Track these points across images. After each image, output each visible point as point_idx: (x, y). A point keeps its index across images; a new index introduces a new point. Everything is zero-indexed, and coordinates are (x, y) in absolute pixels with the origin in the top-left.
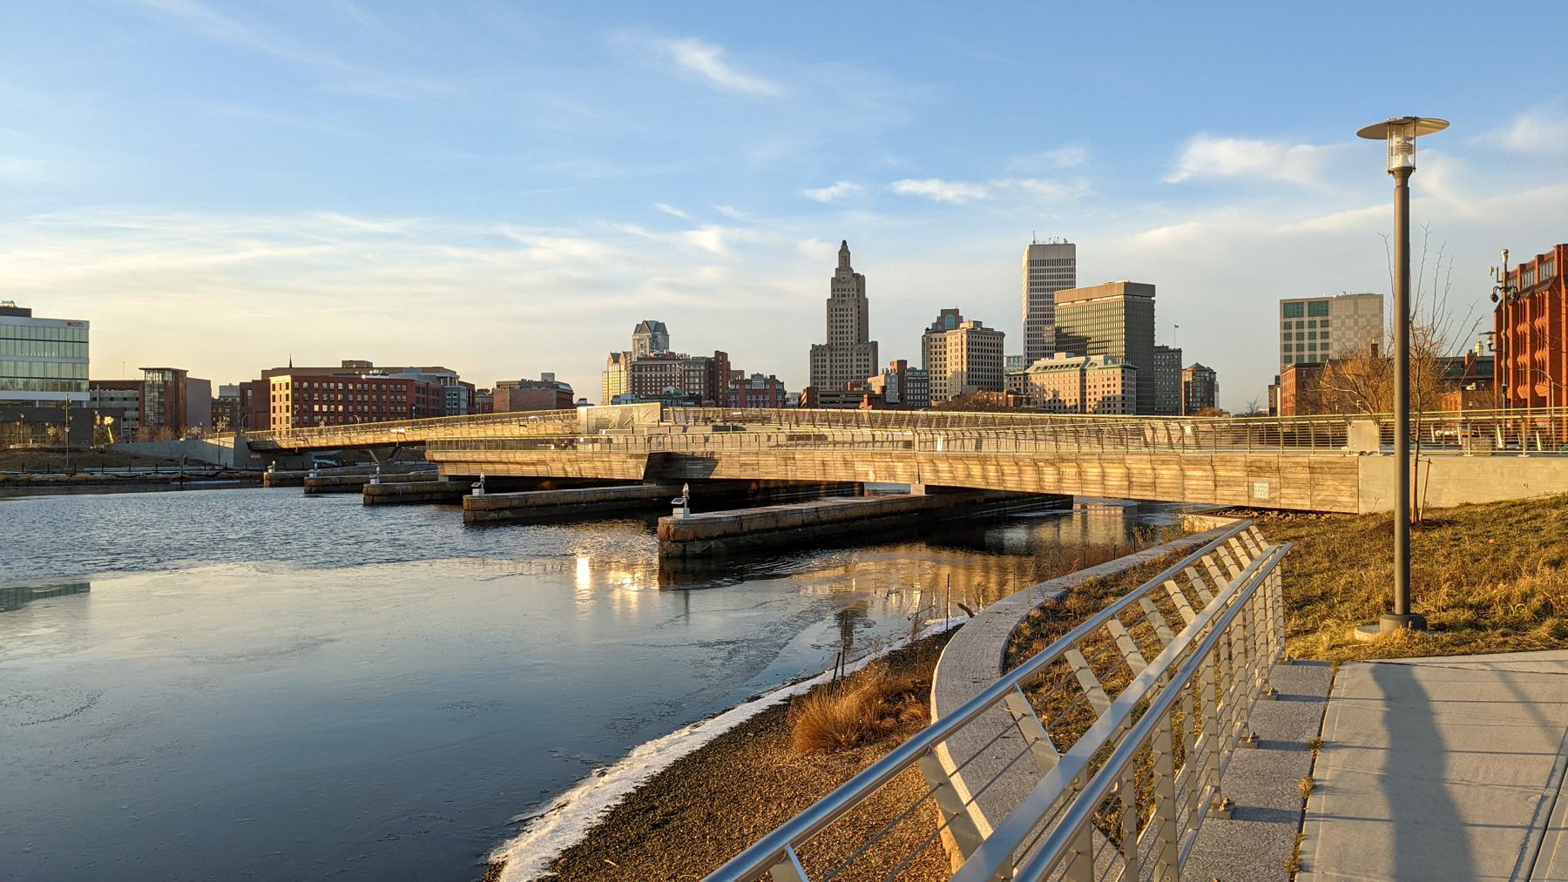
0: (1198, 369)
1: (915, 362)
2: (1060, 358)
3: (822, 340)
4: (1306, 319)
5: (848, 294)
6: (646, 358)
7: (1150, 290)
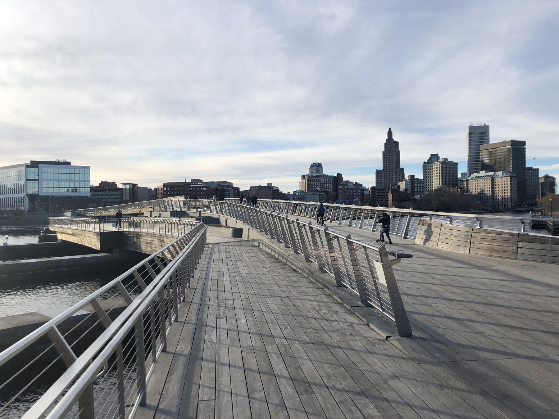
0: (547, 177)
1: (419, 175)
2: (483, 173)
3: (381, 167)
5: (391, 149)
6: (313, 177)
7: (523, 143)
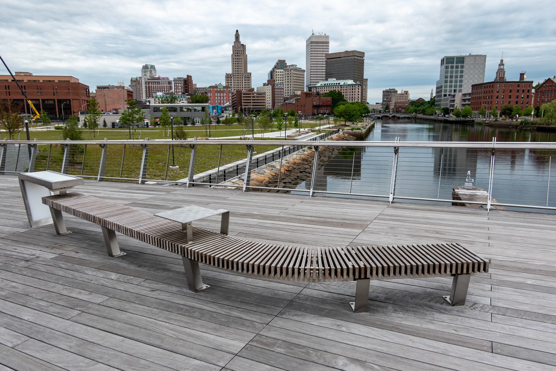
3: (230, 71)
4: (455, 65)
